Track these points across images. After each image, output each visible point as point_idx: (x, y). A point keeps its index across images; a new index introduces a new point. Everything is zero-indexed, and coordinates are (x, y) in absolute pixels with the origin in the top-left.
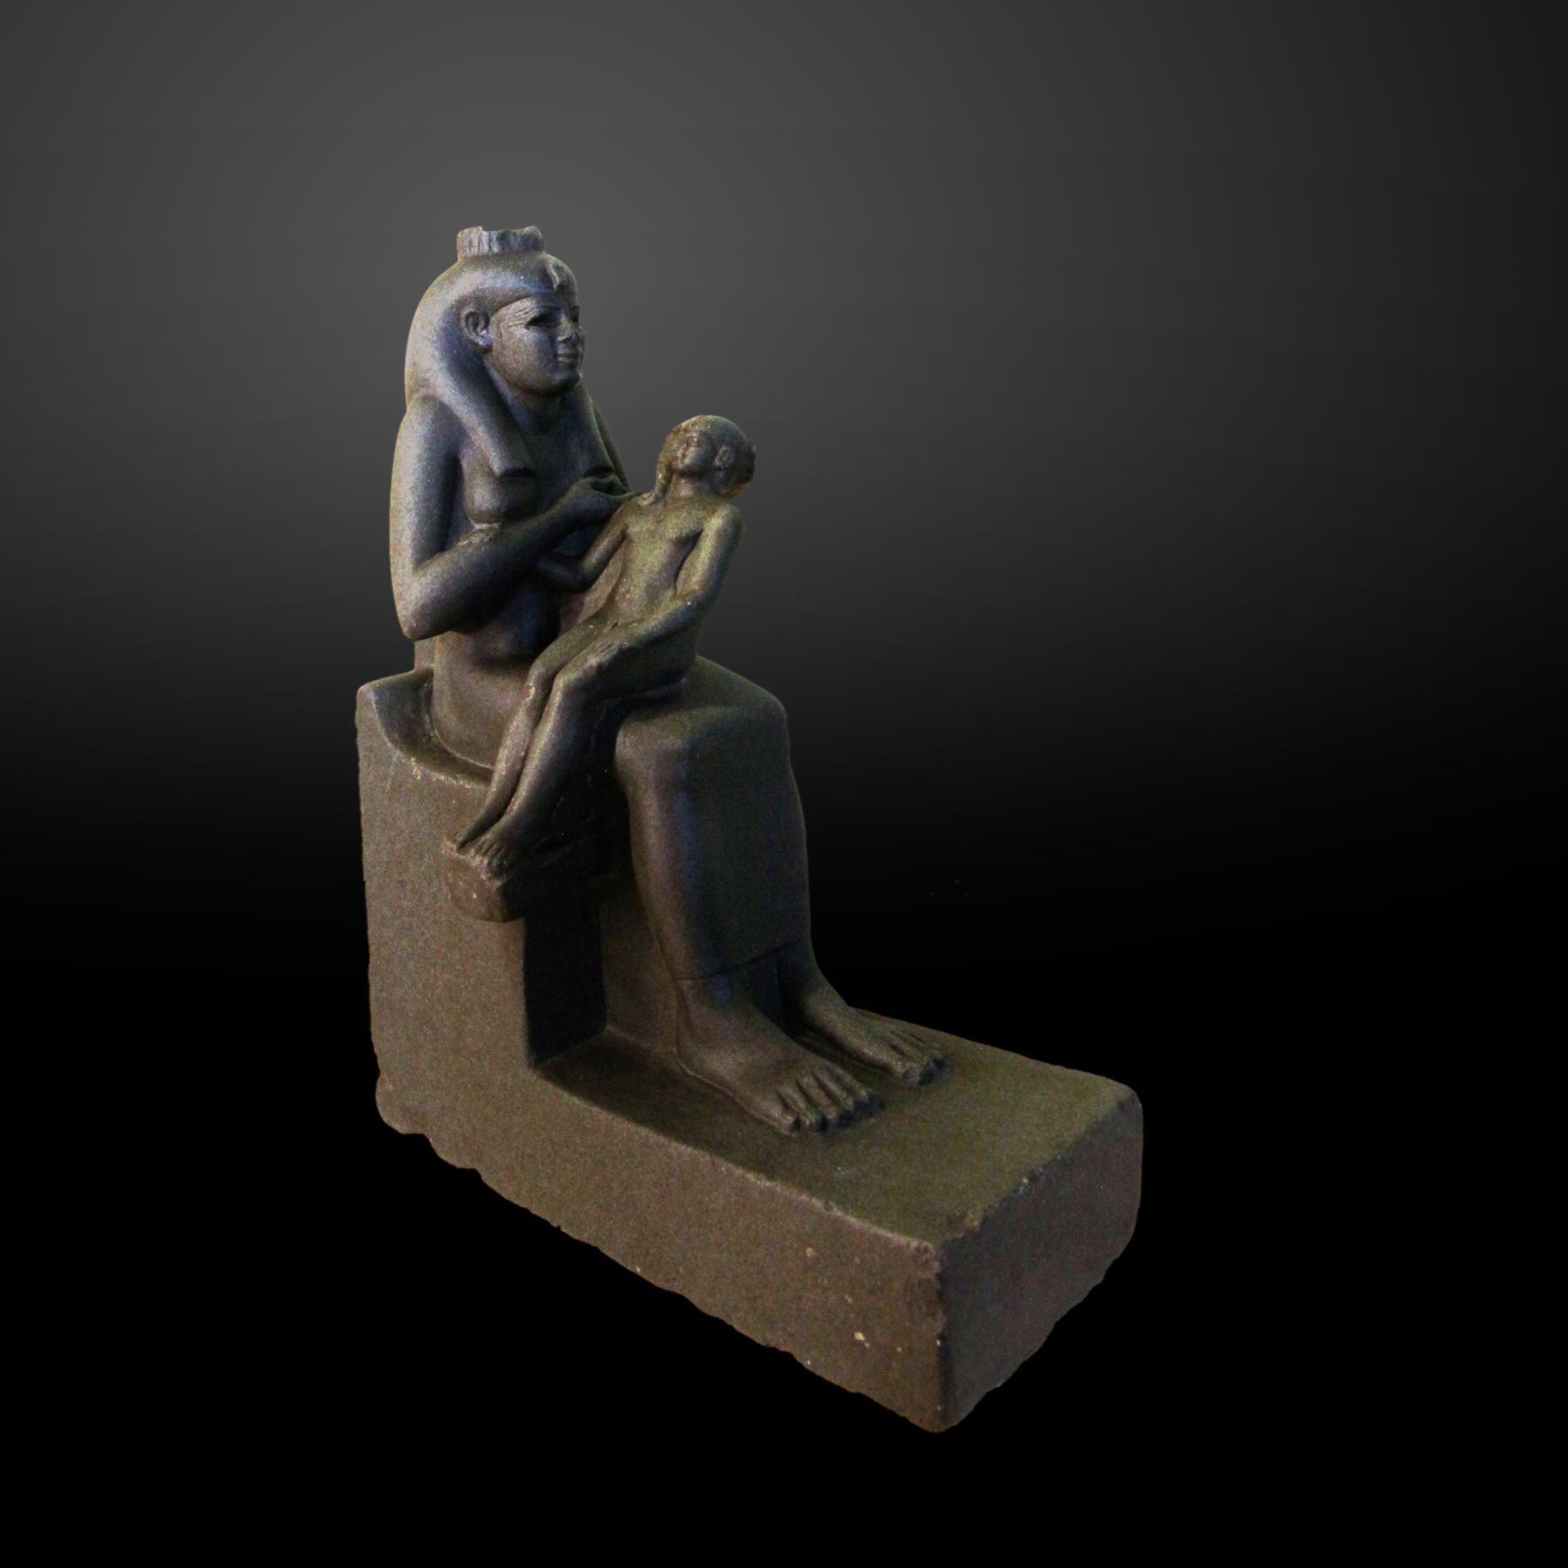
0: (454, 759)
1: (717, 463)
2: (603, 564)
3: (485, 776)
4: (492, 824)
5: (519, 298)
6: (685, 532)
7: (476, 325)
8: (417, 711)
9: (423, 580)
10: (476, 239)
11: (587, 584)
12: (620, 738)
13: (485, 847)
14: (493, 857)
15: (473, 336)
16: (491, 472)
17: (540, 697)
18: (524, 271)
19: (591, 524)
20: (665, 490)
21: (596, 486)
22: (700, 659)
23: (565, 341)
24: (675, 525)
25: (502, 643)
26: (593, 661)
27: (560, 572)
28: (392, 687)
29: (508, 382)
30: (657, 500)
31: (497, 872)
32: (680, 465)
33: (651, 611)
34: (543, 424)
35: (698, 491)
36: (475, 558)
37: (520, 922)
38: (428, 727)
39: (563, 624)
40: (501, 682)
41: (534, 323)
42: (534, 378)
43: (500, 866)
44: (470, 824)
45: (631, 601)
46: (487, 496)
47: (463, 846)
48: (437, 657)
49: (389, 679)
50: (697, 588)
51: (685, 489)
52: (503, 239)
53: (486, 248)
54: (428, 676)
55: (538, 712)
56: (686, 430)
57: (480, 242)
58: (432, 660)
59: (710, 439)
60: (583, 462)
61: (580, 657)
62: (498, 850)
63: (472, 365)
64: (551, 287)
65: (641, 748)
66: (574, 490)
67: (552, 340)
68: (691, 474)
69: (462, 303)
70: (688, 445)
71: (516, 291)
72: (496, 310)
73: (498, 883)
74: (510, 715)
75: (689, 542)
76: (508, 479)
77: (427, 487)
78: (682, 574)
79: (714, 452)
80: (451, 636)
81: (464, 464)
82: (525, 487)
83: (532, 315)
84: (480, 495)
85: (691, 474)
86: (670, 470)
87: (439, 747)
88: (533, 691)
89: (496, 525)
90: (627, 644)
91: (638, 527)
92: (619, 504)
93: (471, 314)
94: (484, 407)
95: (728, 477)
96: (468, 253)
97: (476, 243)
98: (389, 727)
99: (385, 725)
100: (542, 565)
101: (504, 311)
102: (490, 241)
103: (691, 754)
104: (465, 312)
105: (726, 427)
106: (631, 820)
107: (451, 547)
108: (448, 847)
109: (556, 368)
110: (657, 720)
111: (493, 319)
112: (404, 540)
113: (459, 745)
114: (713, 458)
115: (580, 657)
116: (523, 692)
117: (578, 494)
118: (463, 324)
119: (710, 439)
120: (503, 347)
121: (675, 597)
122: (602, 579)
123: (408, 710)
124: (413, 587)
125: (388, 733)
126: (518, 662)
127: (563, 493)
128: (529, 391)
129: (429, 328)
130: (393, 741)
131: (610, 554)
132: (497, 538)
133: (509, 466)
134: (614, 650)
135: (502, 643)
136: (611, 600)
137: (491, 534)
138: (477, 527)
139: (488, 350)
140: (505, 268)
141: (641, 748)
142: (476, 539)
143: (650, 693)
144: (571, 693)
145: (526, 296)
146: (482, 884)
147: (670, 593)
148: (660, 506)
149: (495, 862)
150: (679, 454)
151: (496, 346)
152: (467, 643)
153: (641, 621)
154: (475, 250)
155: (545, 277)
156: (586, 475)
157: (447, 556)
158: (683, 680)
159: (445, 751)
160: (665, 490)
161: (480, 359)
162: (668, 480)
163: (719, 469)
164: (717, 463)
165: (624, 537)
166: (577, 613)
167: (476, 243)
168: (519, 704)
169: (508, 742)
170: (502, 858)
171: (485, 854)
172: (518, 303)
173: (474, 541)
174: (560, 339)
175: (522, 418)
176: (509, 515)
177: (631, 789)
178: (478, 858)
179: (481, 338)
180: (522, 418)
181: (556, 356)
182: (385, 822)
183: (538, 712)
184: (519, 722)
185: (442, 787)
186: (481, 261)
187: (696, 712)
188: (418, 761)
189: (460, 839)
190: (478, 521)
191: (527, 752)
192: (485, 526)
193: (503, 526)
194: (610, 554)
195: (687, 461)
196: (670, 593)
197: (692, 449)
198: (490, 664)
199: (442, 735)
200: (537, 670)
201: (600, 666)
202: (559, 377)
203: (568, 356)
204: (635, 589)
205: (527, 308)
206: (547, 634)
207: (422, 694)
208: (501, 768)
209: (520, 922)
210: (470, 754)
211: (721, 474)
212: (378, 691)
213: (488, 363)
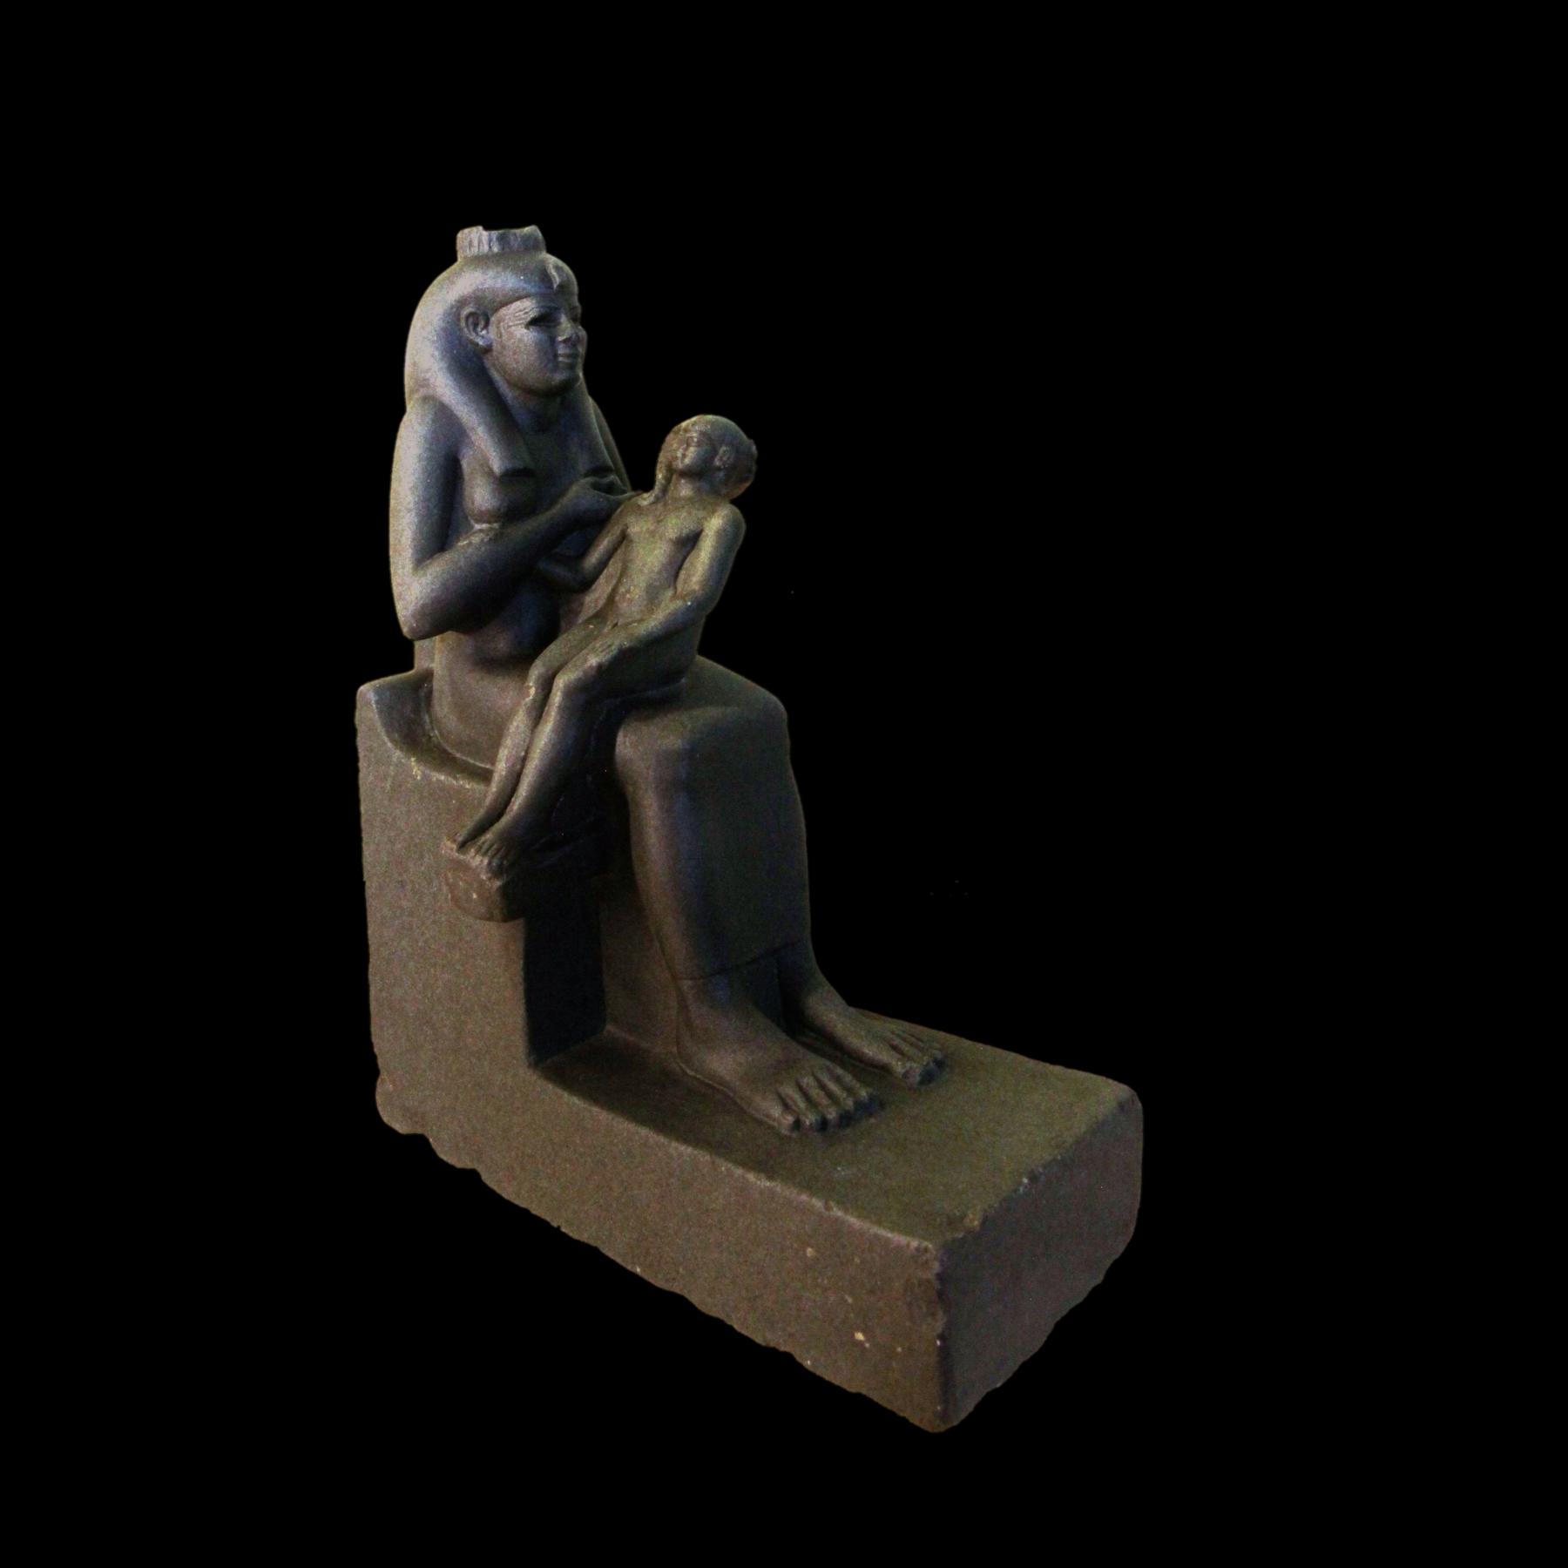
0: (454, 759)
1: (717, 463)
2: (603, 564)
3: (485, 776)
4: (492, 824)
5: (519, 298)
6: (685, 532)
7: (476, 325)
8: (417, 711)
9: (423, 580)
10: (474, 239)
11: (587, 584)
12: (620, 738)
13: (485, 847)
14: (493, 857)
15: (473, 336)
16: (491, 472)
17: (540, 697)
18: (524, 271)
19: (591, 524)
20: (665, 490)
21: (596, 486)
22: (700, 659)
23: (565, 341)
24: (675, 525)
25: (502, 643)
26: (593, 661)
27: (560, 572)
28: (392, 687)
29: (508, 382)
30: (657, 500)
31: (497, 872)
32: (680, 465)
33: (651, 611)
34: (543, 424)
35: (698, 491)
36: (475, 558)
37: (520, 922)
38: (428, 727)
39: (563, 624)
40: (501, 682)
41: (534, 323)
42: (534, 378)
43: (500, 866)
44: (470, 824)
45: (631, 601)
46: (487, 496)
47: (463, 846)
48: (437, 657)
49: (389, 678)
50: (697, 588)
51: (685, 489)
52: (501, 239)
53: (486, 248)
54: (428, 676)
55: (538, 712)
56: (686, 430)
57: (480, 242)
58: (432, 660)
59: (710, 439)
60: (583, 462)
61: (580, 657)
62: (498, 850)
63: (472, 365)
64: (551, 287)
65: (641, 748)
66: (574, 490)
67: (552, 340)
68: (691, 474)
69: (462, 303)
70: (688, 445)
71: (516, 291)
72: (496, 310)
73: (498, 883)
74: (510, 715)
75: (689, 542)
76: (508, 479)
77: (427, 487)
78: (682, 574)
79: (714, 452)
80: (451, 636)
81: (464, 464)
82: (525, 487)
83: (532, 315)
84: (480, 495)
85: (691, 474)
86: (671, 470)
87: (439, 747)
88: (533, 691)
89: (496, 525)
90: (627, 644)
91: (638, 527)
92: (619, 504)
93: (471, 314)
94: (484, 407)
95: (728, 477)
96: (468, 253)
97: (476, 243)
98: (389, 727)
99: (385, 725)
100: (542, 565)
101: (504, 311)
102: (490, 241)
103: (691, 754)
104: (465, 312)
105: (726, 427)
106: (631, 820)
107: (451, 547)
108: (448, 847)
109: (556, 368)
110: (657, 720)
111: (493, 319)
112: (404, 540)
113: (459, 745)
114: (713, 458)
115: (580, 657)
116: (523, 692)
117: (578, 494)
118: (463, 324)
119: (710, 439)
120: (503, 347)
121: (675, 597)
122: (602, 579)
123: (408, 710)
124: (412, 587)
125: (388, 733)
126: (518, 662)
127: (563, 493)
128: (529, 391)
129: (429, 328)
130: (393, 741)
131: (610, 554)
132: (497, 538)
133: (509, 466)
134: (614, 650)
135: (502, 643)
136: (611, 600)
137: (491, 534)
138: (477, 527)
139: (488, 350)
140: (505, 268)
141: (641, 748)
142: (476, 539)
143: (650, 693)
144: (571, 693)
145: (526, 296)
146: (482, 884)
147: (670, 593)
148: (660, 506)
149: (495, 862)
150: (679, 454)
151: (496, 346)
152: (467, 643)
153: (641, 621)
154: (475, 250)
155: (545, 277)
156: (586, 475)
157: (447, 556)
158: (683, 680)
159: (445, 751)
160: (665, 490)
161: (480, 359)
162: (668, 480)
163: (719, 469)
164: (717, 463)
165: (624, 537)
166: (577, 613)
167: (476, 243)
168: (519, 704)
169: (508, 742)
170: (502, 858)
171: (485, 854)
172: (518, 303)
173: (474, 541)
174: (560, 339)
175: (522, 418)
176: (509, 515)
177: (631, 789)
178: (478, 858)
179: (481, 338)
180: (522, 418)
181: (556, 356)
182: (385, 822)
183: (538, 712)
184: (519, 722)
185: (442, 787)
186: (481, 261)
187: (696, 712)
188: (418, 761)
189: (460, 839)
190: (478, 521)
191: (527, 752)
192: (485, 526)
193: (503, 526)
194: (610, 554)
195: (687, 461)
196: (670, 593)
197: (692, 449)
198: (490, 664)
199: (442, 735)
200: (537, 670)
201: (600, 666)
202: (559, 377)
203: (568, 356)
204: (635, 589)
205: (527, 308)
206: (547, 634)
207: (422, 694)
208: (501, 768)
209: (520, 922)
210: (470, 754)
211: (721, 474)
212: (378, 691)
213: (488, 363)
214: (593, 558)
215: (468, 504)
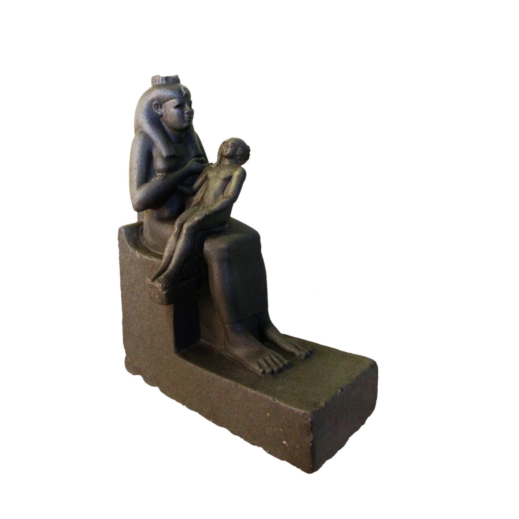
0: (150, 251)
1: (237, 153)
2: (200, 187)
3: (161, 257)
4: (163, 273)
5: (172, 99)
6: (227, 176)
7: (157, 108)
8: (138, 235)
9: (140, 192)
11: (194, 193)
12: (205, 244)
13: (161, 280)
14: (163, 284)
15: (156, 111)
16: (162, 156)
17: (179, 231)
18: (173, 90)
21: (197, 161)
23: (187, 113)
25: (166, 213)
26: (196, 219)
27: (185, 189)
29: (168, 126)
31: (164, 289)
32: (225, 154)
33: (216, 202)
34: (180, 140)
35: (231, 162)
36: (157, 185)
37: (172, 305)
38: (142, 241)
39: (186, 207)
40: (166, 226)
41: (177, 107)
42: (177, 125)
43: (166, 287)
44: (155, 273)
45: (209, 199)
46: (161, 164)
47: (153, 280)
48: (145, 218)
50: (231, 194)
51: (227, 162)
53: (161, 82)
55: (178, 236)
57: (159, 80)
58: (143, 219)
59: (235, 145)
60: (193, 153)
61: (192, 217)
62: (165, 281)
64: (182, 95)
65: (212, 248)
66: (190, 162)
67: (183, 113)
69: (153, 100)
70: (228, 147)
71: (171, 96)
72: (164, 103)
73: (165, 292)
74: (169, 237)
75: (228, 179)
76: (168, 159)
77: (141, 161)
78: (226, 190)
79: (236, 150)
80: (149, 211)
81: (154, 153)
82: (174, 161)
83: (176, 104)
84: (159, 164)
87: (145, 247)
88: (176, 229)
89: (164, 174)
90: (207, 213)
92: (205, 167)
93: (156, 104)
94: (160, 135)
95: (241, 158)
97: (157, 80)
99: (127, 240)
100: (179, 187)
101: (167, 103)
103: (229, 250)
104: (154, 103)
106: (209, 271)
107: (149, 181)
108: (148, 281)
109: (184, 122)
110: (217, 238)
111: (163, 106)
113: (152, 246)
114: (236, 152)
116: (173, 229)
117: (191, 164)
118: (153, 107)
119: (235, 145)
120: (167, 115)
121: (223, 198)
122: (199, 192)
123: (135, 235)
125: (129, 243)
126: (172, 219)
127: (186, 163)
128: (175, 129)
129: (142, 109)
130: (130, 245)
131: (202, 183)
132: (164, 178)
133: (169, 154)
134: (203, 215)
135: (166, 213)
136: (202, 198)
137: (163, 177)
138: (158, 174)
139: (161, 116)
140: (167, 89)
142: (157, 179)
143: (215, 229)
144: (189, 229)
145: (174, 98)
146: (159, 292)
147: (222, 196)
148: (218, 168)
149: (164, 285)
150: (225, 150)
152: (155, 213)
153: (212, 205)
154: (157, 83)
156: (194, 157)
157: (148, 184)
158: (226, 225)
159: (147, 249)
161: (159, 119)
163: (238, 155)
164: (237, 153)
165: (206, 178)
166: (191, 203)
167: (157, 80)
168: (172, 233)
169: (168, 246)
170: (166, 284)
171: (160, 283)
172: (171, 100)
173: (157, 179)
174: (185, 112)
175: (173, 138)
176: (169, 170)
177: (209, 261)
178: (158, 284)
179: (159, 112)
180: (173, 138)
181: (184, 118)
182: (127, 272)
183: (178, 236)
184: (172, 239)
185: (146, 260)
187: (230, 236)
188: (138, 252)
189: (152, 278)
190: (158, 173)
191: (174, 249)
192: (160, 174)
193: (166, 174)
194: (202, 183)
195: (227, 153)
196: (222, 196)
197: (229, 149)
198: (162, 220)
199: (146, 243)
200: (178, 222)
201: (199, 221)
202: (185, 125)
203: (188, 118)
204: (210, 195)
205: (175, 102)
206: (181, 210)
207: (140, 230)
208: (166, 254)
209: (172, 305)
210: (155, 250)
211: (239, 157)
213: (161, 120)
214: (196, 185)
215: (155, 167)
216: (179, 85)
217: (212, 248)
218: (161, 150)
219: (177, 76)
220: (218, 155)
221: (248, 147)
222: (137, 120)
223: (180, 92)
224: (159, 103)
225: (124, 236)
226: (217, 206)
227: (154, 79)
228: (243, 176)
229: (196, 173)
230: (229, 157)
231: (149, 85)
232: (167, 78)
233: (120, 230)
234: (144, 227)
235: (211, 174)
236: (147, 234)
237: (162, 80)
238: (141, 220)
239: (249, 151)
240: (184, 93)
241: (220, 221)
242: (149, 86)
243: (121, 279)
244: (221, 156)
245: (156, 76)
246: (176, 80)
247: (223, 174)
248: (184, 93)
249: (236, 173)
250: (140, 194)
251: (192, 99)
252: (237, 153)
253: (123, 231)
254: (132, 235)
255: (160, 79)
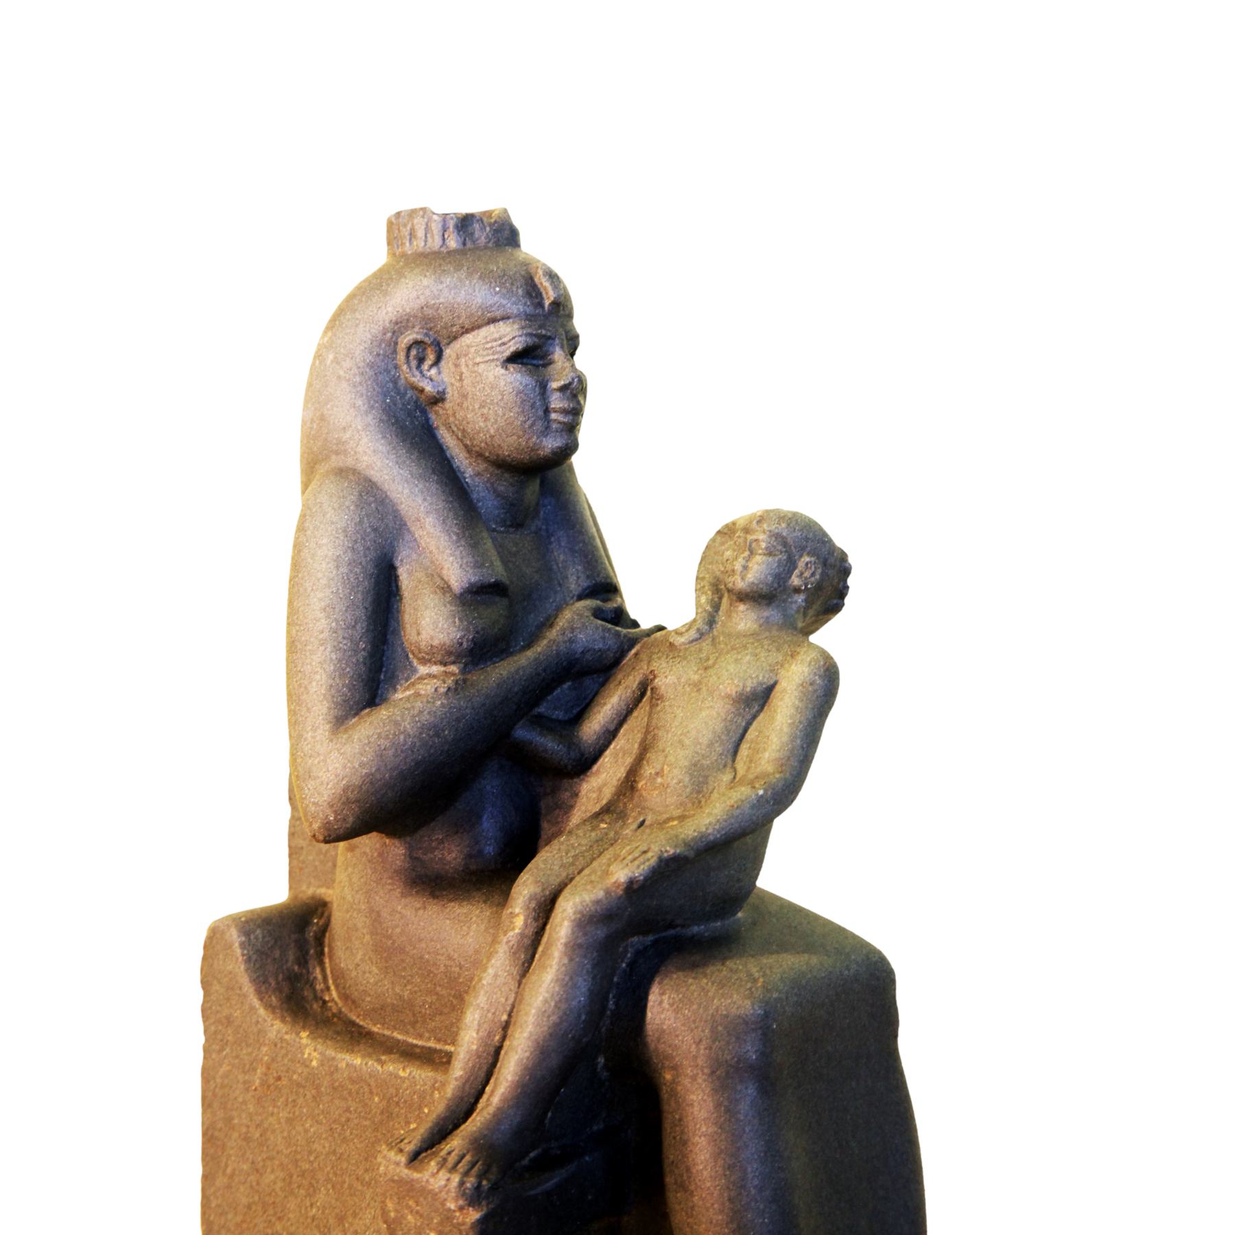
0: (369, 1035)
1: (795, 581)
2: (610, 735)
3: (438, 1060)
4: (456, 1126)
5: (493, 321)
6: (750, 686)
7: (421, 360)
8: (303, 961)
9: (348, 749)
11: (585, 763)
12: (654, 997)
13: (452, 1159)
14: (466, 1174)
15: (416, 379)
16: (446, 588)
17: (530, 931)
21: (598, 614)
23: (563, 389)
25: (450, 854)
26: (621, 874)
27: (549, 744)
29: (468, 449)
31: (474, 1198)
32: (740, 584)
33: (698, 805)
34: (516, 517)
35: (766, 624)
36: (425, 717)
39: (545, 825)
40: (459, 909)
41: (516, 358)
42: (511, 444)
43: (478, 1188)
44: (417, 1131)
45: (664, 787)
46: (443, 623)
47: (415, 1158)
48: (341, 876)
50: (770, 769)
51: (744, 619)
55: (530, 951)
57: (427, 229)
58: (330, 883)
59: (785, 543)
60: (575, 580)
61: (590, 867)
62: (473, 1165)
64: (541, 305)
65: (683, 1015)
66: (566, 617)
67: (543, 386)
69: (400, 325)
70: (752, 553)
71: (488, 309)
72: (454, 338)
73: (474, 1215)
74: (478, 964)
75: (759, 699)
76: (478, 595)
77: (352, 606)
78: (744, 750)
79: (791, 564)
80: (370, 843)
81: (403, 573)
82: (499, 612)
83: (512, 347)
84: (430, 621)
87: (339, 1016)
88: (519, 922)
89: (454, 668)
93: (417, 343)
94: (434, 487)
95: (809, 603)
97: (420, 233)
98: (261, 982)
99: (254, 981)
100: (522, 733)
101: (468, 339)
103: (765, 1026)
106: (667, 1125)
107: (384, 700)
108: (392, 1162)
109: (546, 431)
111: (448, 352)
112: (314, 687)
113: (379, 1012)
114: (790, 573)
116: (497, 925)
117: (572, 624)
118: (401, 356)
119: (785, 543)
120: (465, 396)
122: (607, 758)
125: (260, 994)
126: (492, 875)
127: (549, 623)
129: (347, 364)
130: (269, 1007)
131: (623, 718)
132: (458, 688)
134: (652, 860)
135: (450, 854)
136: (629, 784)
138: (423, 670)
139: (438, 399)
140: (470, 275)
142: (427, 688)
144: (586, 922)
145: (505, 318)
146: (448, 1217)
147: (726, 777)
148: (706, 645)
149: (471, 1182)
152: (396, 850)
153: (682, 818)
154: (419, 244)
156: (580, 597)
158: (740, 915)
159: (353, 1024)
161: (424, 412)
163: (797, 590)
164: (795, 581)
165: (644, 688)
166: (568, 809)
167: (420, 233)
168: (495, 941)
170: (480, 1177)
171: (453, 1169)
172: (492, 327)
173: (423, 694)
174: (555, 385)
175: (487, 502)
176: (478, 652)
178: (443, 1175)
179: (428, 380)
180: (487, 502)
181: (547, 411)
182: (247, 1139)
183: (530, 951)
184: (498, 967)
185: (358, 1079)
189: (410, 1148)
190: (424, 661)
192: (436, 669)
194: (623, 718)
195: (751, 577)
196: (726, 777)
197: (758, 558)
198: (430, 883)
199: (345, 997)
200: (526, 888)
201: (631, 882)
202: (551, 444)
203: (565, 412)
204: (669, 771)
205: (511, 336)
206: (520, 848)
207: (311, 933)
208: (469, 1041)
210: (400, 1025)
211: (800, 599)
216: (521, 257)
217: (683, 1015)
218: (438, 562)
219: (505, 211)
220: (699, 590)
221: (843, 557)
222: (322, 418)
223: (532, 291)
224: (431, 344)
225: (237, 967)
226: (709, 819)
227: (399, 228)
228: (825, 688)
229: (588, 672)
230: (761, 597)
231: (374, 255)
232: (465, 223)
233: (214, 939)
234: (338, 917)
235: (670, 677)
236: (352, 957)
237: (445, 230)
238: (312, 890)
239: (846, 571)
240: (549, 296)
241: (697, 903)
242: (377, 256)
243: (207, 1178)
244: (718, 592)
245: (413, 213)
246: (505, 234)
247: (736, 673)
248: (549, 296)
249: (795, 677)
250: (351, 756)
251: (580, 323)
252: (801, 579)
253: (235, 937)
254: (284, 955)
255: (436, 228)
